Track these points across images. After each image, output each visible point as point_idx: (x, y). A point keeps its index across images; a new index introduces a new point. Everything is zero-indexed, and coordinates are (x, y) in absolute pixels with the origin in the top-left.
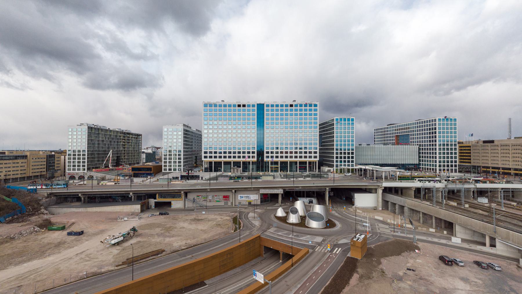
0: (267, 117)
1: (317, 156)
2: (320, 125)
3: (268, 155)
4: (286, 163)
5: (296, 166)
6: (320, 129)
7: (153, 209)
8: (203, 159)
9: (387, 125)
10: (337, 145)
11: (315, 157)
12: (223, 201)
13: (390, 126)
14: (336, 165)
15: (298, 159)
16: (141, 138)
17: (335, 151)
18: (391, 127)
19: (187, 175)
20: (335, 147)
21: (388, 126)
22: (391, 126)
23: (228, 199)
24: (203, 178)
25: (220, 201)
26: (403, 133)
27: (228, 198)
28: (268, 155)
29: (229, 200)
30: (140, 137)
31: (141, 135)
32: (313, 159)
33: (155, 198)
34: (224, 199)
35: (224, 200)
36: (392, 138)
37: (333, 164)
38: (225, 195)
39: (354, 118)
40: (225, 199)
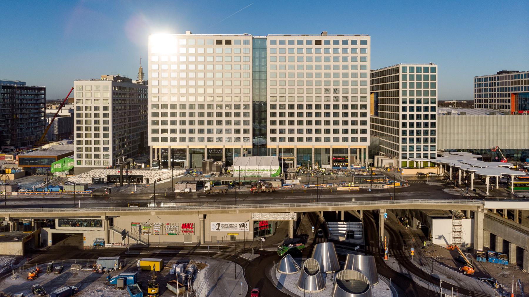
0: (272, 71)
1: (366, 121)
2: (372, 75)
3: (273, 119)
4: (308, 151)
5: (327, 155)
6: (372, 82)
7: (57, 218)
8: (150, 143)
9: (498, 73)
10: (404, 93)
11: (364, 140)
12: (182, 233)
13: (502, 75)
14: (403, 139)
15: (332, 145)
16: (44, 94)
17: (401, 105)
18: (503, 77)
19: (119, 174)
20: (401, 97)
21: (499, 76)
22: (505, 75)
23: (190, 230)
24: (150, 180)
25: (176, 234)
26: (516, 90)
27: (192, 228)
28: (273, 119)
29: (193, 232)
30: (43, 92)
31: (44, 89)
32: (359, 145)
33: (53, 227)
34: (182, 230)
35: (185, 232)
36: (505, 81)
37: (397, 121)
38: (187, 222)
39: (436, 66)
40: (185, 229)
